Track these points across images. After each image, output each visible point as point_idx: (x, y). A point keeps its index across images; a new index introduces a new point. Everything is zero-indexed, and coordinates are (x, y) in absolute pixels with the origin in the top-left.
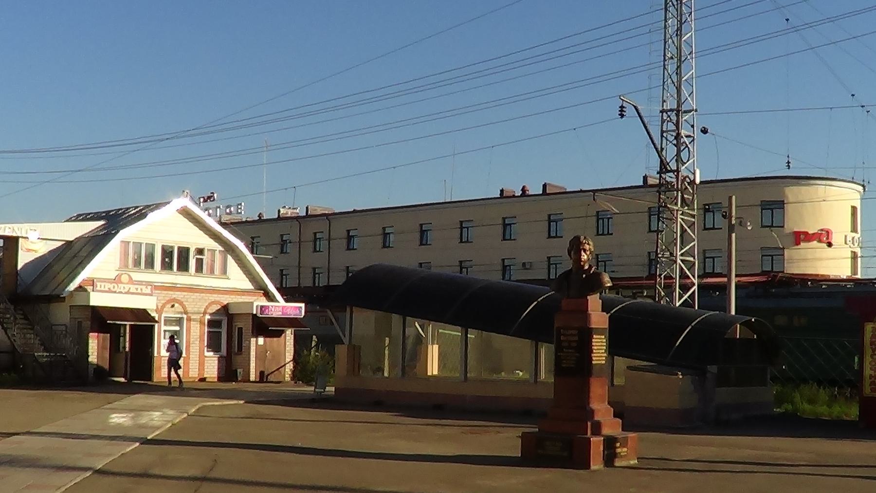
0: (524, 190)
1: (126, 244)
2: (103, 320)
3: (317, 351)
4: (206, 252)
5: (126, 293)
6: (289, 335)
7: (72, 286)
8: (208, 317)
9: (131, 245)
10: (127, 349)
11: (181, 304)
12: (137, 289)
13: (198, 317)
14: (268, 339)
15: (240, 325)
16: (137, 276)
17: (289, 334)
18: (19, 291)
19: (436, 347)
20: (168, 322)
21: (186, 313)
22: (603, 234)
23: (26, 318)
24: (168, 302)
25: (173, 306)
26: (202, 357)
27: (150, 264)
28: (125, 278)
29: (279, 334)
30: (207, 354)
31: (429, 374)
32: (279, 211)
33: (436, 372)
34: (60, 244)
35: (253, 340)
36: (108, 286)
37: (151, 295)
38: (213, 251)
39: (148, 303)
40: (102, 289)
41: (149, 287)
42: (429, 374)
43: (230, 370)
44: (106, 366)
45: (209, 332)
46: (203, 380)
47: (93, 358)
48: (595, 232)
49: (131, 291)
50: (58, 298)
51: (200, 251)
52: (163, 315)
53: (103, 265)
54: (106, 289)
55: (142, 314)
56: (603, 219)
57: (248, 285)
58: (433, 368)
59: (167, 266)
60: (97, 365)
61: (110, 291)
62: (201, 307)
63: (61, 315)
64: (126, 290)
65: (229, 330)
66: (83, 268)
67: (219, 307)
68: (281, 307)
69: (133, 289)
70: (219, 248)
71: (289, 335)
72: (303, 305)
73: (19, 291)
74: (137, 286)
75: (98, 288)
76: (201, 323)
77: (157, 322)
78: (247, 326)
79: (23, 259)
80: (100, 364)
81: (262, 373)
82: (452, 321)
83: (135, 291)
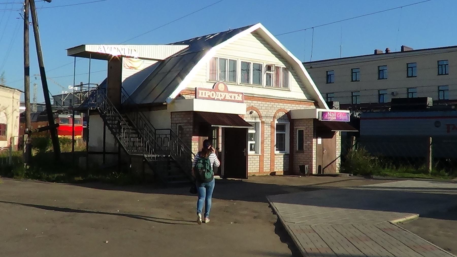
0: (387, 50)
2: (204, 123)
3: (356, 147)
6: (338, 136)
7: (173, 95)
8: (276, 122)
10: (220, 150)
13: (269, 120)
17: (338, 136)
18: (123, 101)
21: (260, 117)
22: (442, 74)
23: (130, 124)
25: (251, 113)
26: (272, 155)
27: (233, 78)
28: (221, 87)
34: (155, 62)
35: (314, 140)
36: (208, 94)
37: (242, 102)
38: (277, 68)
39: (239, 109)
40: (204, 96)
41: (241, 95)
43: (293, 166)
45: (277, 134)
46: (273, 174)
48: (437, 73)
50: (161, 106)
51: (269, 68)
53: (197, 77)
54: (207, 96)
56: (442, 65)
57: (303, 96)
59: (246, 80)
61: (209, 98)
62: (270, 114)
63: (162, 120)
64: (223, 98)
66: (182, 78)
69: (228, 97)
70: (282, 65)
72: (348, 111)
73: (123, 101)
74: (230, 94)
76: (272, 127)
77: (251, 126)
78: (308, 129)
79: (126, 74)
81: (320, 167)
83: (230, 99)
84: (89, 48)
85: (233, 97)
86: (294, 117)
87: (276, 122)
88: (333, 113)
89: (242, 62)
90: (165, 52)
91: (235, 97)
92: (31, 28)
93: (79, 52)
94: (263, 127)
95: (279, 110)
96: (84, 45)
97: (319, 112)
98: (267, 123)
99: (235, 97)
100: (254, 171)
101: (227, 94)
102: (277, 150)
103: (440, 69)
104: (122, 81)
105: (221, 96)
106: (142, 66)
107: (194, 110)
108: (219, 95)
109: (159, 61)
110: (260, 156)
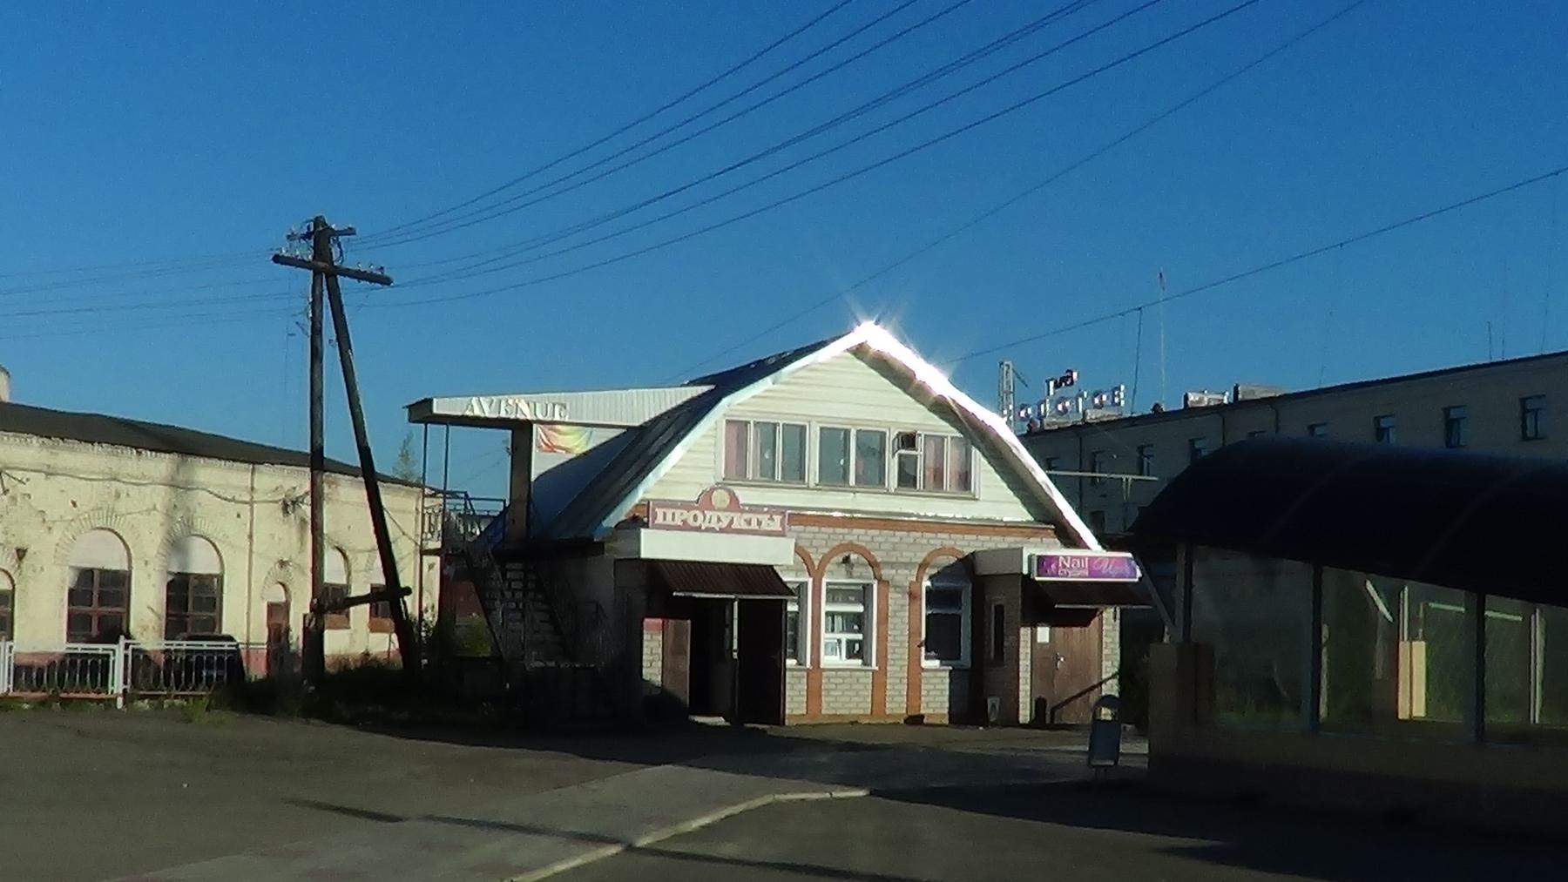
1: (738, 427)
2: (667, 587)
4: (920, 442)
5: (722, 531)
6: (1109, 621)
7: (611, 521)
8: (926, 583)
9: (751, 427)
11: (863, 552)
12: (749, 522)
13: (905, 577)
14: (1059, 631)
15: (999, 599)
16: (746, 496)
19: (1420, 647)
20: (835, 594)
24: (834, 551)
25: (846, 560)
26: (914, 671)
28: (720, 498)
29: (1083, 619)
30: (925, 664)
31: (1403, 714)
32: (1186, 398)
33: (1419, 711)
35: (1025, 633)
36: (680, 516)
37: (781, 534)
41: (778, 518)
42: (1403, 714)
43: (977, 694)
44: (684, 693)
46: (915, 720)
47: (652, 671)
49: (735, 526)
50: (590, 548)
51: (908, 440)
52: (825, 580)
55: (764, 576)
57: (1017, 512)
58: (1413, 701)
60: (662, 688)
61: (685, 527)
64: (724, 524)
65: (974, 607)
67: (953, 560)
68: (1091, 557)
69: (739, 523)
71: (1109, 621)
74: (746, 516)
75: (659, 520)
76: (913, 596)
77: (790, 593)
78: (1011, 600)
79: (541, 464)
80: (669, 687)
82: (1441, 575)
83: (744, 526)
84: (438, 408)
85: (754, 522)
86: (982, 570)
87: (926, 583)
88: (1080, 558)
89: (822, 429)
90: (643, 405)
91: (759, 523)
92: (331, 354)
93: (421, 412)
94: (883, 598)
95: (941, 551)
96: (430, 401)
97: (1030, 558)
98: (896, 587)
99: (759, 523)
100: (854, 712)
101: (736, 516)
102: (927, 658)
103: (1530, 422)
104: (533, 477)
105: (719, 519)
106: (576, 443)
107: (643, 555)
108: (714, 519)
109: (629, 428)
110: (874, 672)
